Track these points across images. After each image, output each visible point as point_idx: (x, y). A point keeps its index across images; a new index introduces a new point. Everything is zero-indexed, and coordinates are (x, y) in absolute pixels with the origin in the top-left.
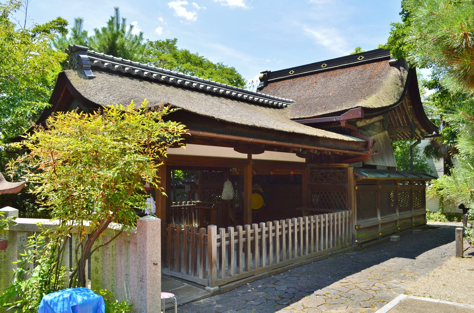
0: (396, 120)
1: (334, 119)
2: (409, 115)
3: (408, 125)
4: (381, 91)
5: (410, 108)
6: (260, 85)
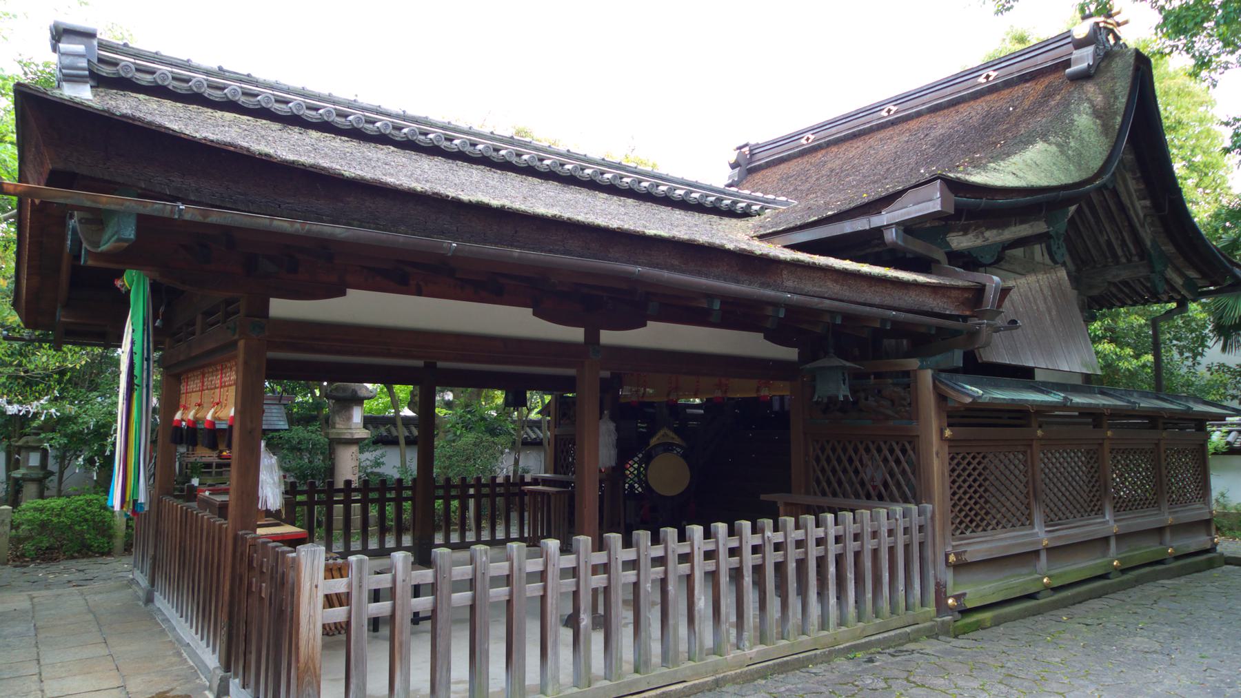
0: (1105, 247)
2: (1143, 226)
5: (1144, 207)
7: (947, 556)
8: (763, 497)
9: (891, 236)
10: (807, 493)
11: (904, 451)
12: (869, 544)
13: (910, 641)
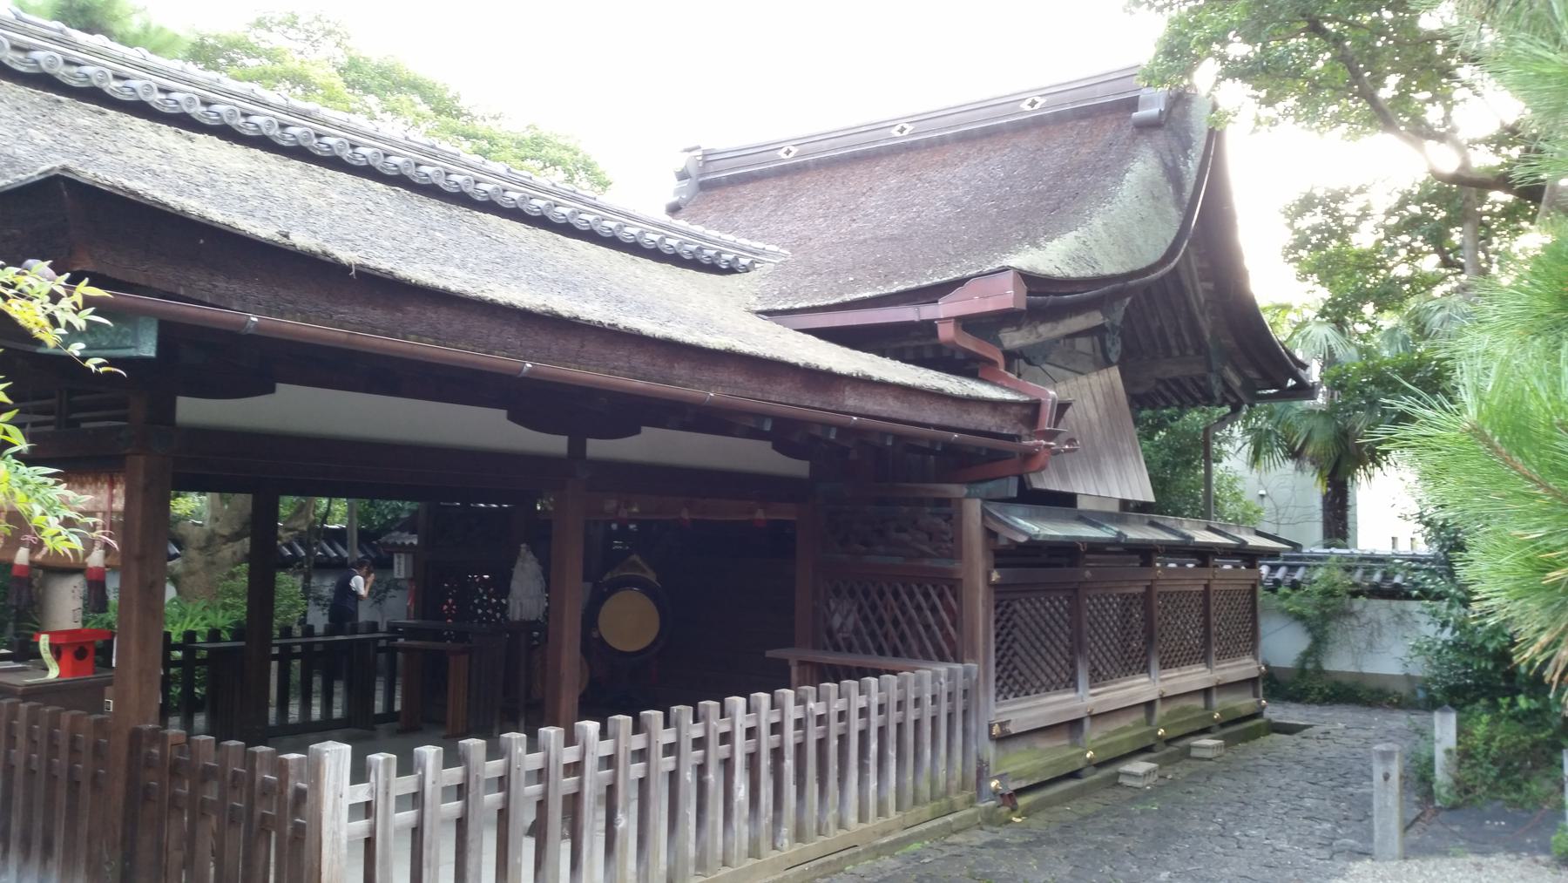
1: (907, 314)
2: (1203, 313)
3: (1198, 352)
4: (1097, 222)
5: (1206, 291)
6: (677, 192)
7: (991, 727)
8: (769, 654)
9: (946, 333)
10: (815, 647)
11: (941, 596)
12: (912, 715)
13: (956, 832)
